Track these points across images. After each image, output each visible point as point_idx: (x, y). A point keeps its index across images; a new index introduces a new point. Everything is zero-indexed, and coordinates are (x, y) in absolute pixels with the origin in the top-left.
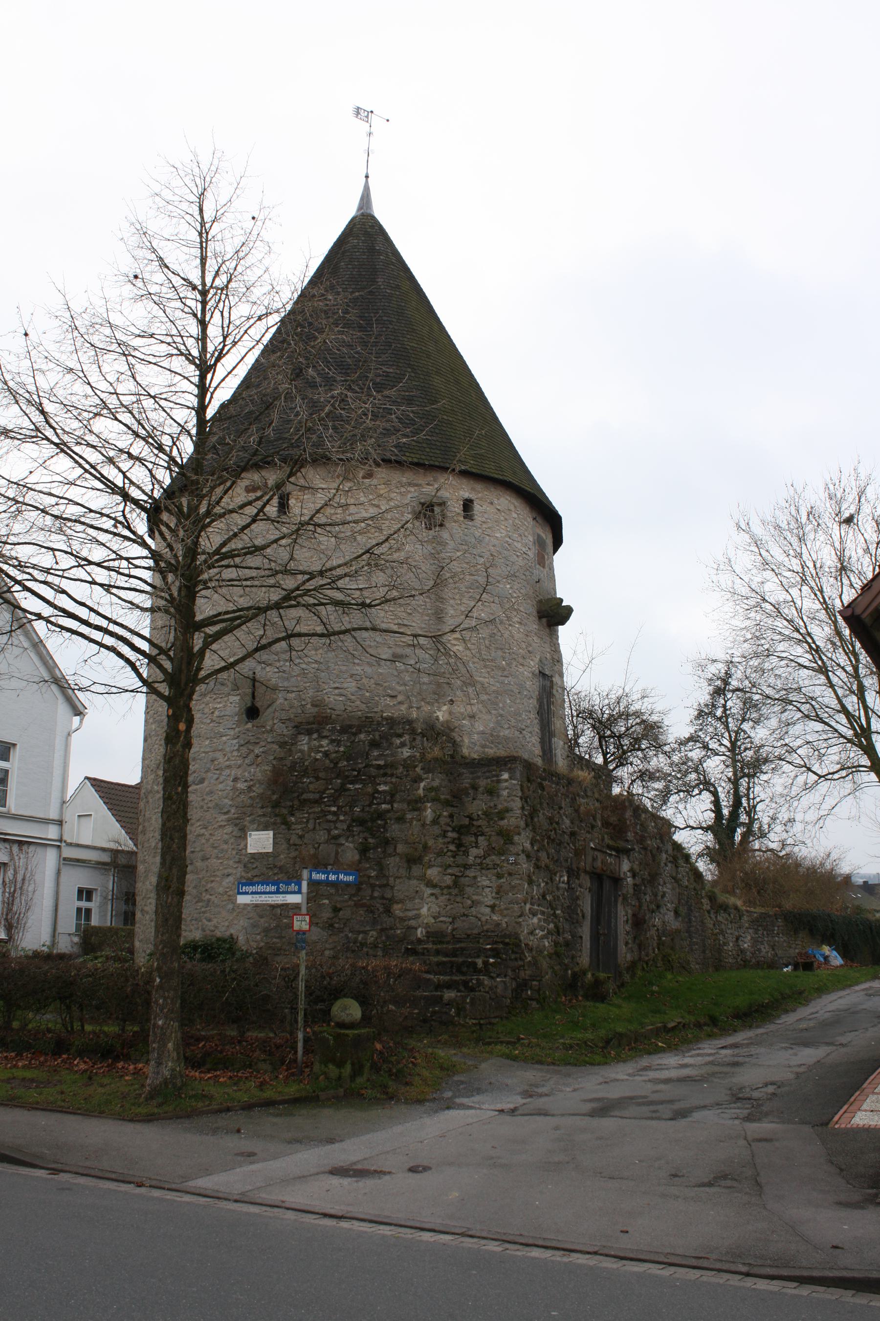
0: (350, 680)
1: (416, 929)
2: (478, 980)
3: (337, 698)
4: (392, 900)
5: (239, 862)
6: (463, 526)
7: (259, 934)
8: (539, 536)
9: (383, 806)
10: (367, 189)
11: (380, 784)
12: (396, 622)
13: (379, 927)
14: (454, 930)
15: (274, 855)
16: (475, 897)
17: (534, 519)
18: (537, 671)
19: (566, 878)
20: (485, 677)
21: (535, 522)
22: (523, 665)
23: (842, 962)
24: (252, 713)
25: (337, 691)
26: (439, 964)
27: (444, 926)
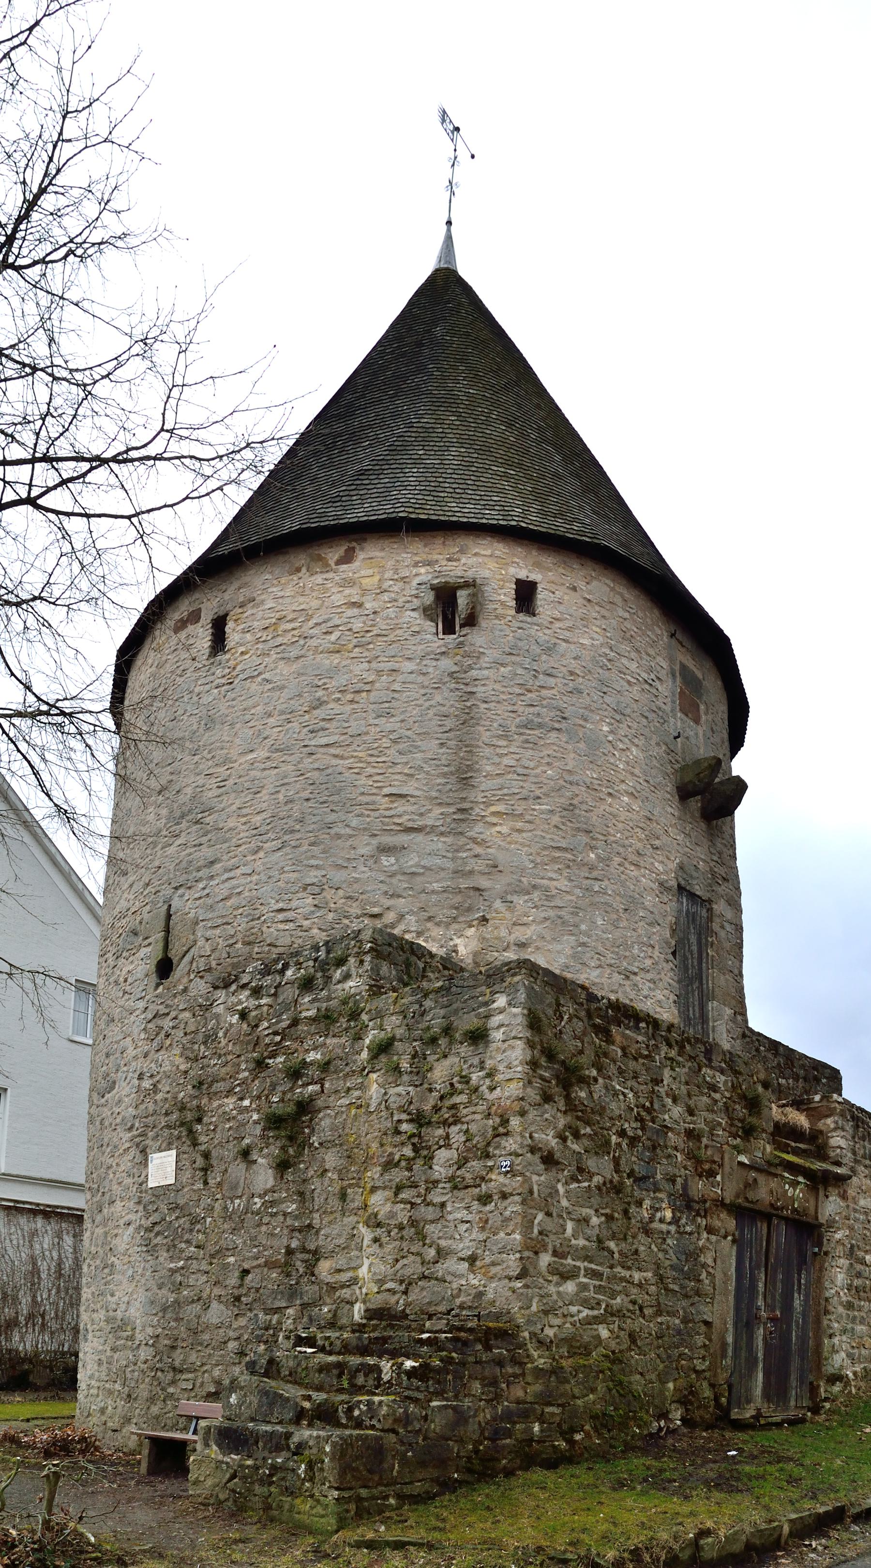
0: (304, 895)
1: (352, 1304)
2: (370, 1404)
3: (281, 926)
4: (317, 1255)
5: (139, 1203)
6: (515, 624)
7: (156, 1314)
8: (683, 667)
9: (310, 1088)
10: (449, 239)
11: (307, 1051)
12: (386, 791)
13: (298, 1302)
14: (407, 1304)
15: (176, 1188)
16: (443, 1243)
17: (672, 635)
18: (673, 883)
19: (668, 1214)
20: (551, 879)
21: (673, 641)
22: (637, 865)
23: (151, 1184)
24: (165, 968)
25: (281, 916)
26: (323, 1368)
27: (393, 1299)
